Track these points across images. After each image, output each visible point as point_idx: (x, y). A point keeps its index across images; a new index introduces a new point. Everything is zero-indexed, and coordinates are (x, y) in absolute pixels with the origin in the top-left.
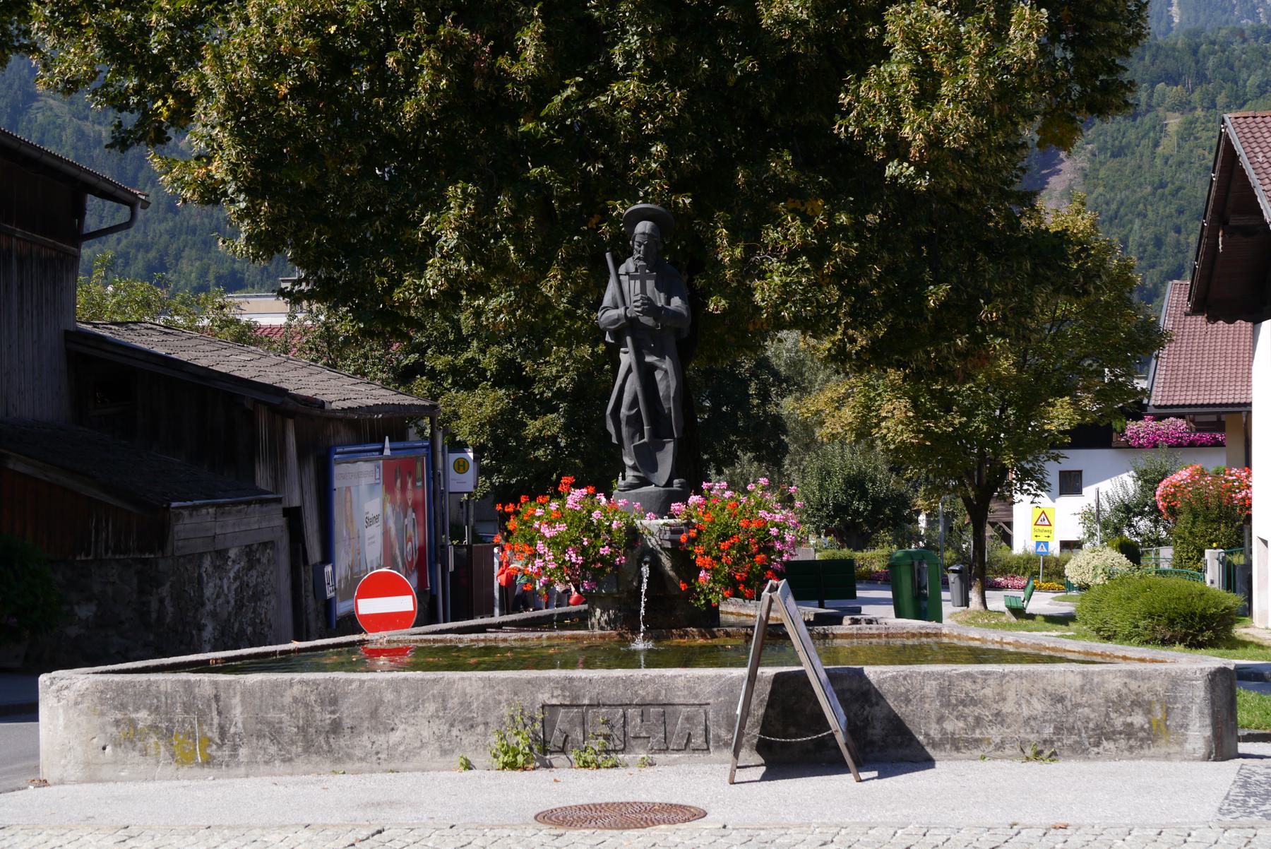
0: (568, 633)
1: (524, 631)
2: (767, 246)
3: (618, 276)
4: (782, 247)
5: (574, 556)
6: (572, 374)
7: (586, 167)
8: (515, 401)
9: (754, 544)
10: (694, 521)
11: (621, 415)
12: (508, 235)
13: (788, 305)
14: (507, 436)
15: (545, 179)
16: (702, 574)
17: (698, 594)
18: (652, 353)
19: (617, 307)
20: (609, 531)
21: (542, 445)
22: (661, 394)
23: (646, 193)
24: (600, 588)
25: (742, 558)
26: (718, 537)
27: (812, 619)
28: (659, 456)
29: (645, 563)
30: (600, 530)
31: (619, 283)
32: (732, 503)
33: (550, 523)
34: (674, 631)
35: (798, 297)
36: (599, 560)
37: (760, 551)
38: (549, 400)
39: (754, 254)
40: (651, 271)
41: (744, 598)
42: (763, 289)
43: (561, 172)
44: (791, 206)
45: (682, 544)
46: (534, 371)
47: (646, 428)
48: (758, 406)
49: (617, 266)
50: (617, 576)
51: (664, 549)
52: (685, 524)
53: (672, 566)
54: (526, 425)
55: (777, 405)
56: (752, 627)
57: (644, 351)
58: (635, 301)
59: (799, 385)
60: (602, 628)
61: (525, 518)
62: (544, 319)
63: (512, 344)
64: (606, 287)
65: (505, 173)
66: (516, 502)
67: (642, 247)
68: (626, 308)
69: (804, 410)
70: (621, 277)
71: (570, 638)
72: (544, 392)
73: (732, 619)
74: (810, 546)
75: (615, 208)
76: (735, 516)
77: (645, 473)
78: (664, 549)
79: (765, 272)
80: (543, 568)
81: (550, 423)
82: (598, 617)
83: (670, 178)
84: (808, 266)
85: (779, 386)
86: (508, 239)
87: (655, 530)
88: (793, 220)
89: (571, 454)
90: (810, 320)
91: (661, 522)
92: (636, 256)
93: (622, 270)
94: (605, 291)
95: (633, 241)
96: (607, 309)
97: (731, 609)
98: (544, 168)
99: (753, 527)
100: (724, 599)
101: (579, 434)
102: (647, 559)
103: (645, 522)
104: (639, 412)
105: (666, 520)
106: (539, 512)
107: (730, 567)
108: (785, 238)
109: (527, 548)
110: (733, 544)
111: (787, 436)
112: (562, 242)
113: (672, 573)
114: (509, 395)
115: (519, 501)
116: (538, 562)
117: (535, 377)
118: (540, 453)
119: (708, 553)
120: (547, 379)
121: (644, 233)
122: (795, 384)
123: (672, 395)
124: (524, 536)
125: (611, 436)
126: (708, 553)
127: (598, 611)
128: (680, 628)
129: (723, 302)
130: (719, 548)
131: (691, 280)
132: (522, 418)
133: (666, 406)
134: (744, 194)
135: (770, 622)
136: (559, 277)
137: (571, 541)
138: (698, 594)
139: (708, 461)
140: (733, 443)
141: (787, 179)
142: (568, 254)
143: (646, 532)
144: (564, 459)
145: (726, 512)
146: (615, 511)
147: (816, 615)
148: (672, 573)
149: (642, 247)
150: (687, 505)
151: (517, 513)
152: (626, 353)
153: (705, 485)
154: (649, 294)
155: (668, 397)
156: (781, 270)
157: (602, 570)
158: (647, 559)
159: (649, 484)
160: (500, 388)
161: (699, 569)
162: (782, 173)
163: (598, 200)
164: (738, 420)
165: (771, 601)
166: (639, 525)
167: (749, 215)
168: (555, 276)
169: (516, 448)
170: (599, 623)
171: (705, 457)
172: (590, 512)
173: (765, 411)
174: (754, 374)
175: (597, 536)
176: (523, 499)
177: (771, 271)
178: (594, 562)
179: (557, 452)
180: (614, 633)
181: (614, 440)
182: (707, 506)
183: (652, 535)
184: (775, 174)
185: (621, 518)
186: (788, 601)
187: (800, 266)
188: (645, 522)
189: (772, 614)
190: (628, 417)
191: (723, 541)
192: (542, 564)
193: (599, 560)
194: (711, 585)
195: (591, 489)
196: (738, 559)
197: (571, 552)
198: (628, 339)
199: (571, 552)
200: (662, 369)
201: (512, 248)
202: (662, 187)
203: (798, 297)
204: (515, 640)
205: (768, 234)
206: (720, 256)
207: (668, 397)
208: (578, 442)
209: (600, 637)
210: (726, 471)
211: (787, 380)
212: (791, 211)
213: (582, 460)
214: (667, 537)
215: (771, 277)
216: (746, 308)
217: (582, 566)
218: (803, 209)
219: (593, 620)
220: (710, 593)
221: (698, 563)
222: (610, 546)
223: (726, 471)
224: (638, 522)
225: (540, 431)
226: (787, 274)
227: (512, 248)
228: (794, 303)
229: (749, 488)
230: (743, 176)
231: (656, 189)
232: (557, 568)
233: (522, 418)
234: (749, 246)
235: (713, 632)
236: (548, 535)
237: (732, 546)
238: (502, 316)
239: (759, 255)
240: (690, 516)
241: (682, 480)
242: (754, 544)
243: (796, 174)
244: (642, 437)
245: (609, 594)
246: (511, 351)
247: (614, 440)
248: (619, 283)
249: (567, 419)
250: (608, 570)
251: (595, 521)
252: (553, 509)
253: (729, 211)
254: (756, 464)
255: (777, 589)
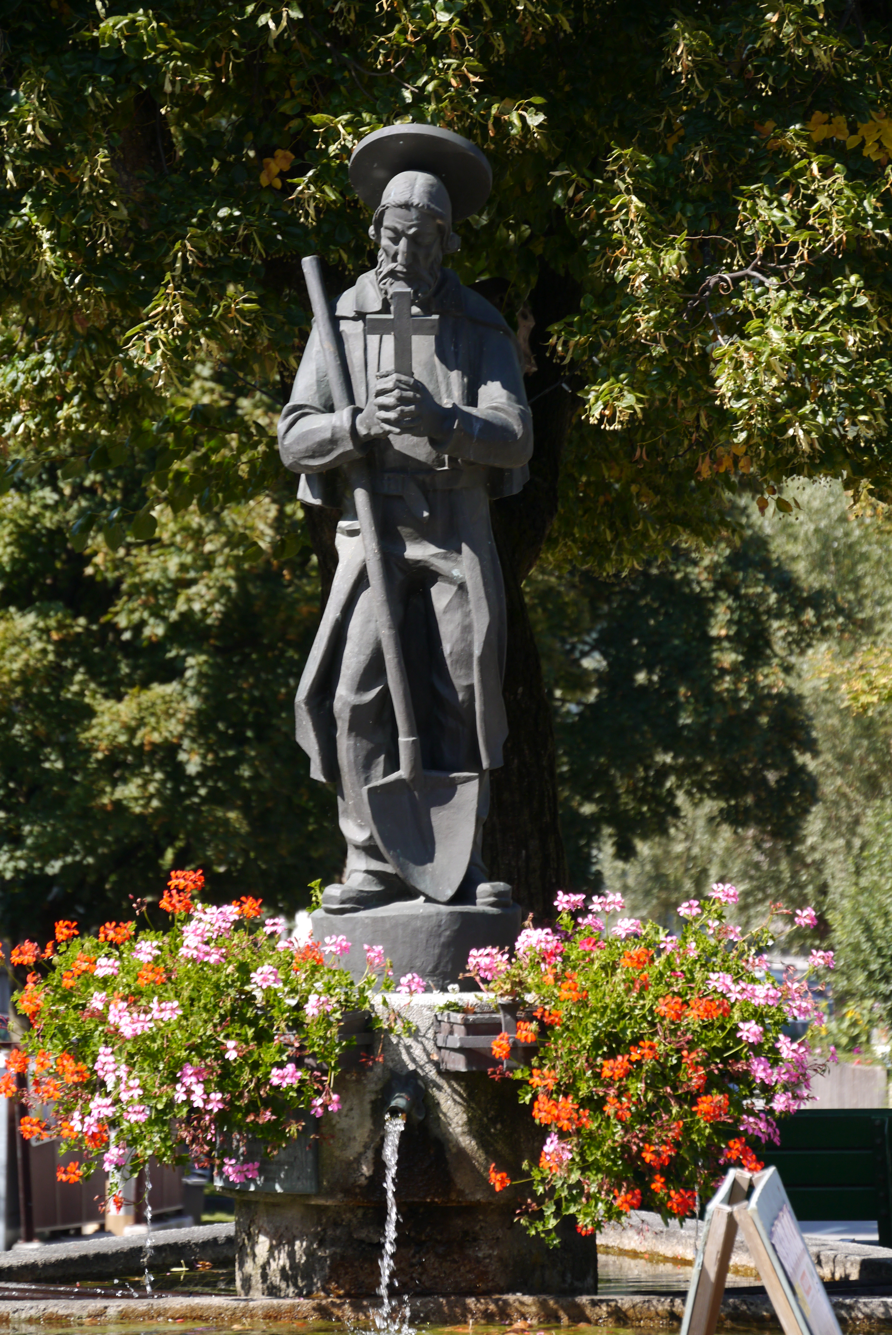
0: (176, 1303)
1: (57, 1295)
2: (752, 246)
3: (335, 321)
4: (794, 247)
5: (198, 1089)
6: (223, 575)
7: (255, 16)
8: (64, 647)
9: (696, 1065)
10: (530, 998)
11: (337, 705)
12: (36, 198)
13: (807, 409)
14: (39, 742)
15: (141, 48)
16: (551, 1145)
17: (540, 1200)
18: (425, 534)
19: (329, 408)
20: (297, 1025)
21: (134, 770)
22: (447, 648)
23: (420, 97)
24: (270, 1180)
25: (661, 1104)
26: (597, 1044)
27: (854, 1276)
28: (439, 817)
29: (395, 1112)
30: (271, 1019)
31: (339, 340)
32: (635, 951)
33: (133, 998)
34: (471, 1301)
35: (834, 386)
36: (268, 1103)
37: (710, 1084)
38: (158, 646)
39: (715, 265)
40: (427, 311)
41: (667, 1214)
42: (738, 365)
43: (184, 29)
44: (820, 133)
45: (497, 1062)
46: (117, 564)
47: (404, 740)
48: (735, 670)
49: (332, 294)
50: (316, 1147)
51: (449, 1075)
52: (505, 1008)
53: (470, 1122)
54: (91, 713)
55: (788, 669)
56: (683, 1294)
57: (404, 531)
58: (381, 393)
59: (849, 617)
60: (272, 1291)
61: (68, 983)
62: (139, 433)
63: (57, 489)
64: (302, 349)
65: (29, 27)
66: (44, 936)
67: (403, 242)
68: (357, 411)
69: (860, 685)
70: (344, 326)
71: (184, 1318)
72: (143, 623)
73: (636, 1270)
74: (874, 1061)
75: (332, 135)
76: (645, 987)
77: (400, 865)
78: (449, 1075)
79: (746, 316)
80: (114, 1123)
81: (160, 708)
82: (260, 1260)
83: (485, 51)
84: (862, 300)
85: (795, 616)
86: (37, 208)
87: (422, 1022)
88: (827, 172)
89: (216, 798)
90: (868, 450)
91: (439, 999)
92: (386, 266)
93: (346, 304)
94: (299, 359)
95: (379, 224)
96: (301, 411)
97: (631, 1241)
98: (140, 16)
99: (693, 1018)
100: (614, 1214)
101: (239, 741)
102: (400, 1101)
103: (398, 999)
104: (385, 697)
105: (454, 995)
106: (105, 967)
107: (627, 1129)
108: (802, 223)
109: (70, 1065)
110: (639, 1064)
111: (816, 754)
112: (186, 222)
113: (468, 1143)
114: (46, 631)
115: (52, 936)
116: (100, 1106)
117: (119, 581)
118: (129, 791)
119: (566, 1089)
120: (154, 589)
121: (407, 206)
122: (840, 611)
123: (477, 651)
124: (62, 1031)
125: (307, 760)
126: (566, 1089)
127: (263, 1244)
128: (487, 1293)
129: (630, 399)
130: (597, 1076)
131: (538, 338)
132: (81, 694)
133: (459, 682)
134: (691, 100)
135: (732, 1280)
136: (179, 318)
137: (192, 1048)
138: (540, 1200)
139: (596, 820)
140: (664, 771)
141: (810, 58)
142: (201, 254)
143: (398, 1027)
144: (195, 809)
145: (620, 975)
146: (315, 969)
147: (867, 1265)
148: (468, 1143)
149: (403, 242)
150: (512, 954)
151: (44, 968)
152: (353, 533)
153: (563, 901)
154: (420, 373)
155: (465, 658)
156: (788, 311)
157: (275, 1130)
158: (400, 1101)
159: (410, 893)
160: (23, 609)
161: (543, 1132)
162: (798, 42)
163: (286, 108)
164: (678, 708)
165: (732, 1226)
166: (380, 1009)
167: (705, 158)
168: (167, 317)
169: (65, 777)
170: (264, 1276)
171: (588, 809)
172: (245, 970)
173: (753, 686)
174: (723, 583)
175: (263, 1037)
176: (62, 930)
177: (762, 314)
178: (253, 1108)
179: (175, 789)
180: (306, 1304)
181: (317, 773)
182: (566, 959)
183: (415, 1034)
184: (778, 46)
185: (329, 989)
186: (779, 1229)
187: (843, 300)
188: (398, 999)
189: (737, 1259)
190: (356, 710)
191: (611, 1055)
192: (109, 1112)
193: (268, 1103)
194: (575, 1176)
195: (250, 906)
196: (651, 1106)
197: (189, 1080)
198: (361, 497)
199: (189, 1080)
200: (450, 580)
201: (46, 235)
202: (464, 79)
203: (834, 386)
204: (30, 1321)
205: (754, 212)
206: (621, 272)
207: (465, 658)
208: (236, 762)
209: (267, 1317)
210: (643, 848)
211: (817, 600)
212: (819, 148)
213: (246, 811)
214: (456, 1040)
215: (761, 332)
216: (690, 416)
217: (221, 1118)
218: (852, 142)
219: (249, 1267)
220: (574, 1200)
221: (540, 1116)
222: (299, 1062)
223: (643, 848)
224: (376, 999)
225: (132, 731)
226: (806, 322)
227: (46, 235)
228: (824, 403)
229: (683, 910)
230: (690, 51)
231: (446, 85)
232: (151, 1122)
233: (81, 694)
234: (703, 243)
235: (580, 1308)
236: (127, 1031)
237: (634, 1070)
238: (16, 418)
239: (729, 268)
240: (520, 984)
241: (501, 885)
242: (696, 1065)
243: (835, 43)
244: (393, 765)
245: (291, 1198)
246: (54, 508)
247: (317, 773)
248: (339, 340)
249: (206, 698)
250: (293, 1129)
251: (259, 994)
252: (144, 958)
253: (649, 145)
254: (726, 832)
255: (748, 1196)
